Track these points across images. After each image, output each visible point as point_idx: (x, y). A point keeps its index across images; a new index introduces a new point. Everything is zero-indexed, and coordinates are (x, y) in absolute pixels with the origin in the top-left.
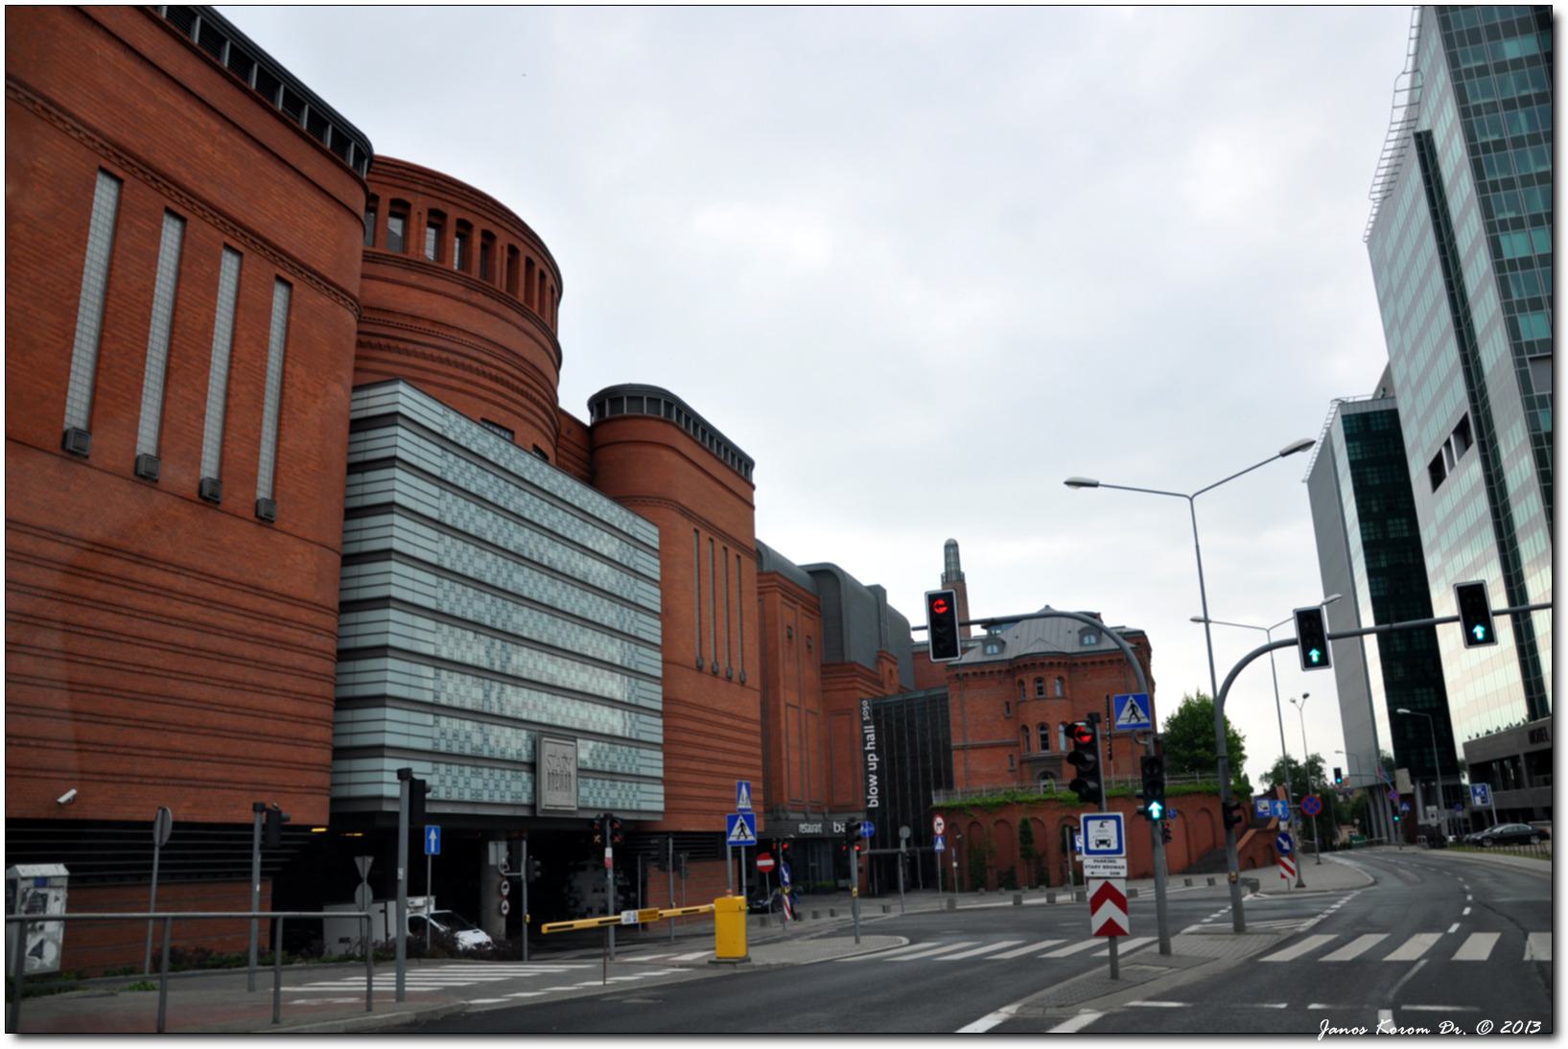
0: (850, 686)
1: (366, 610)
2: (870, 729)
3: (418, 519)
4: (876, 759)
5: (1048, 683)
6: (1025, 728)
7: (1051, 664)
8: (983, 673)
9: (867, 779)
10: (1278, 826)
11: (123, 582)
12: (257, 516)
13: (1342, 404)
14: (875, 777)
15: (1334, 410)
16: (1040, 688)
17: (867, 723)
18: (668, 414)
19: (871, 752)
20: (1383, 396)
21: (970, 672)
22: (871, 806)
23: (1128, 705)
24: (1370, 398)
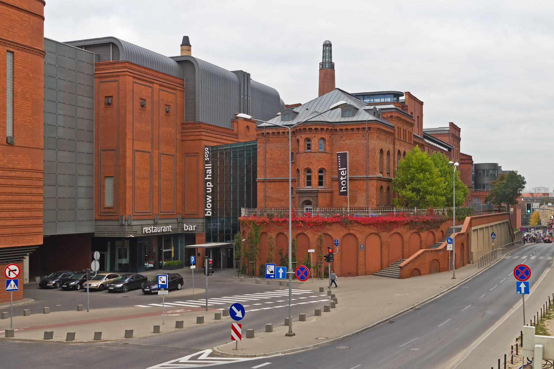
0: (197, 138)
2: (209, 166)
4: (211, 186)
5: (313, 142)
6: (298, 171)
7: (316, 129)
8: (279, 133)
10: (446, 247)
11: (12, 178)
12: (7, 143)
16: (309, 145)
17: (207, 162)
19: (209, 181)
21: (270, 132)
22: (207, 215)
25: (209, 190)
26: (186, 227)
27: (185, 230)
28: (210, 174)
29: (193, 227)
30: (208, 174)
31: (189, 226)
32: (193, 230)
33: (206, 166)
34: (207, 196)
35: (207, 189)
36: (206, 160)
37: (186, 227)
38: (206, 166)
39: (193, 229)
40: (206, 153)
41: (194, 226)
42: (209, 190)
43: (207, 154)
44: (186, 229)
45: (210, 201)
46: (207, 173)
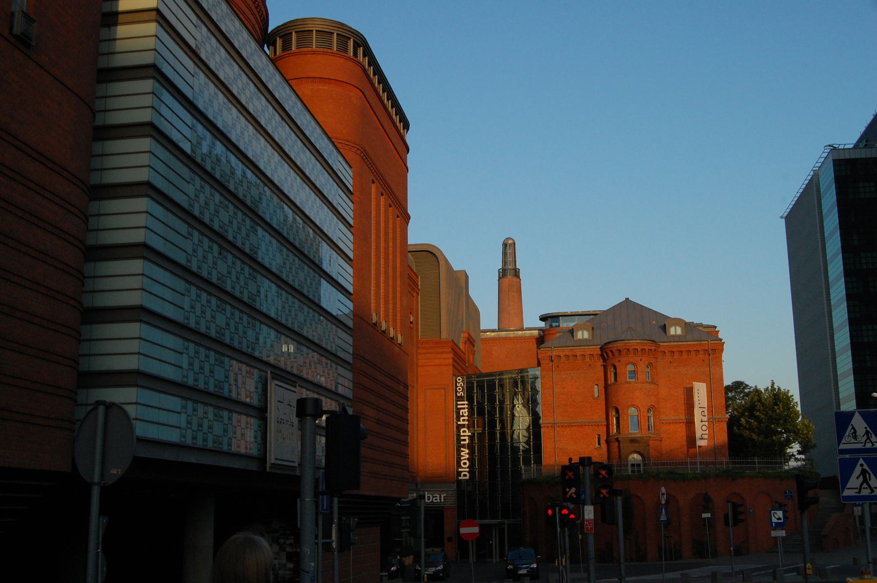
1: (122, 138)
2: (464, 404)
3: (180, 42)
9: (459, 452)
13: (834, 149)
14: (467, 451)
15: (825, 155)
18: (343, 48)
19: (463, 426)
20: (866, 145)
22: (461, 478)
23: (858, 470)
24: (851, 146)
25: (465, 440)
26: (429, 497)
27: (427, 501)
28: (465, 416)
29: (440, 497)
30: (463, 416)
31: (434, 495)
32: (441, 502)
33: (459, 405)
34: (462, 449)
35: (462, 438)
36: (458, 395)
37: (429, 497)
38: (459, 405)
39: (440, 499)
40: (458, 385)
41: (442, 496)
42: (465, 440)
43: (461, 386)
44: (429, 500)
45: (467, 456)
46: (461, 414)
